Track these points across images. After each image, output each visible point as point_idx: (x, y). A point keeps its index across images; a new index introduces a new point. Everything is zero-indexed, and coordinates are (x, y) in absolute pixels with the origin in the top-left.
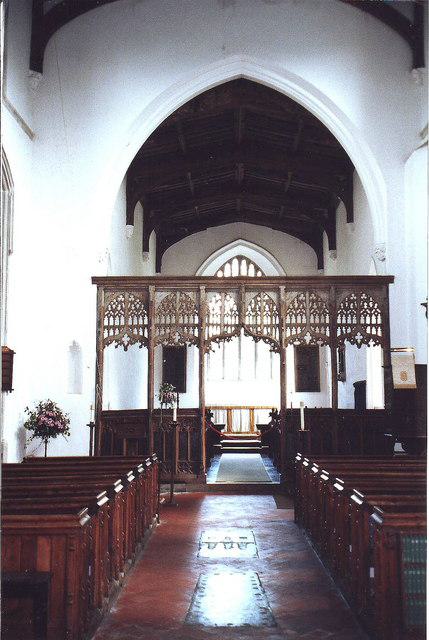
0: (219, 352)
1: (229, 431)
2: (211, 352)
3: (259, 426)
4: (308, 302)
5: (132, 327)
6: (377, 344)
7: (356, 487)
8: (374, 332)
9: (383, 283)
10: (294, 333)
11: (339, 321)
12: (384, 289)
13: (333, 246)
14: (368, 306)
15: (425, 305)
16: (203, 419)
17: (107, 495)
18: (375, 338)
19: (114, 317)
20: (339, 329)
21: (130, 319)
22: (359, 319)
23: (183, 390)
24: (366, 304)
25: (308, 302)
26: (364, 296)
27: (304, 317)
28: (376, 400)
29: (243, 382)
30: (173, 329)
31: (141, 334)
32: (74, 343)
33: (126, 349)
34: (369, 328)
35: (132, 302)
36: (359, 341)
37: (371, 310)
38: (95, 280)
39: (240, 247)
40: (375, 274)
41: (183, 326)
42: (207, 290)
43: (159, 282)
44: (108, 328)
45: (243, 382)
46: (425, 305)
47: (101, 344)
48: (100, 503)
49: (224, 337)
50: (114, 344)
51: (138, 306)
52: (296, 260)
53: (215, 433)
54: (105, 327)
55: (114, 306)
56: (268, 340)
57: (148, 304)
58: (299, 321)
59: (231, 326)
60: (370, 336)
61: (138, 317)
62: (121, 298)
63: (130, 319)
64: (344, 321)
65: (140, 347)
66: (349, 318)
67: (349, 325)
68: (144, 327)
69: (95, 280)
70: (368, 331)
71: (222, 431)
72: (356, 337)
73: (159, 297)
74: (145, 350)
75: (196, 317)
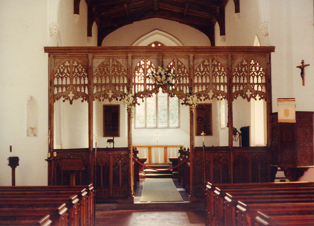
0: (142, 105)
1: (150, 161)
2: (137, 105)
3: (170, 159)
4: (211, 66)
5: (76, 85)
6: (262, 98)
7: (228, 192)
8: (260, 89)
9: (266, 52)
10: (200, 90)
11: (234, 81)
13: (223, 33)
14: (256, 69)
15: (186, 106)
16: (132, 155)
17: (77, 197)
18: (223, 93)
19: (62, 78)
20: (234, 88)
21: (74, 80)
22: (249, 79)
23: (117, 135)
24: (254, 68)
25: (211, 66)
26: (252, 62)
27: (208, 78)
28: (259, 137)
29: (158, 126)
30: (108, 87)
31: (83, 91)
32: (31, 98)
33: (71, 103)
34: (256, 86)
35: (76, 67)
36: (249, 96)
37: (258, 72)
38: (47, 49)
39: (157, 35)
40: (259, 45)
41: (115, 85)
43: (99, 49)
44: (58, 86)
45: (158, 126)
46: (186, 106)
47: (52, 98)
48: (61, 213)
49: (147, 93)
50: (62, 99)
51: (80, 70)
52: (198, 39)
53: (140, 164)
54: (55, 86)
55: (62, 70)
56: (181, 95)
57: (88, 69)
58: (204, 81)
59: (152, 85)
60: (257, 92)
61: (80, 77)
62: (67, 64)
63: (74, 80)
64: (238, 81)
65: (82, 101)
66: (242, 78)
67: (242, 84)
68: (85, 85)
69: (47, 49)
70: (256, 89)
71: (145, 163)
72: (247, 93)
73: (97, 62)
74: (86, 103)
75: (126, 78)
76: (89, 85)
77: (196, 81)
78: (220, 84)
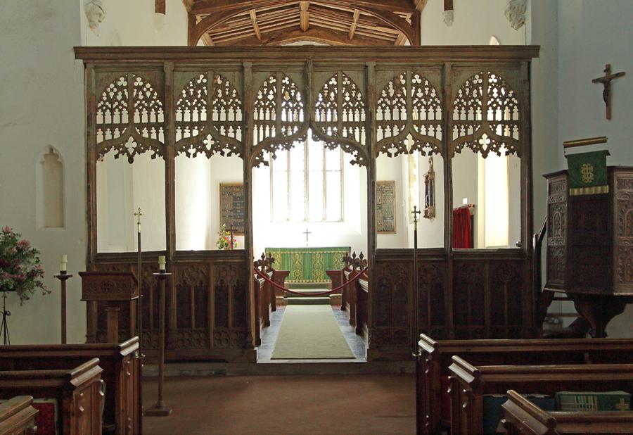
10: (388, 134)
12: (524, 67)
42: (254, 69)
50: (113, 152)
56: (349, 144)
68: (157, 126)
74: (160, 161)
76: (370, 125)
77: (379, 117)
78: (227, 124)
